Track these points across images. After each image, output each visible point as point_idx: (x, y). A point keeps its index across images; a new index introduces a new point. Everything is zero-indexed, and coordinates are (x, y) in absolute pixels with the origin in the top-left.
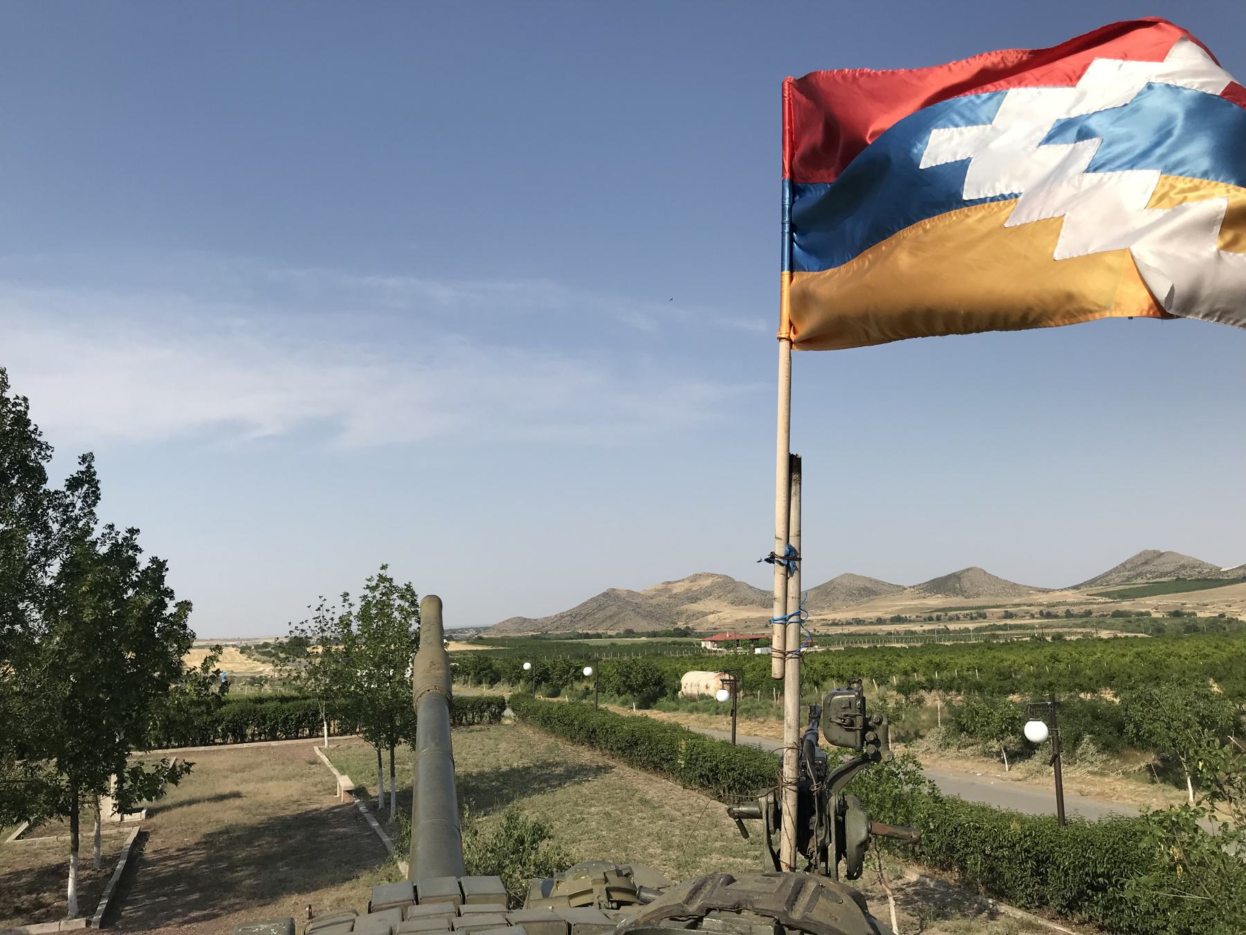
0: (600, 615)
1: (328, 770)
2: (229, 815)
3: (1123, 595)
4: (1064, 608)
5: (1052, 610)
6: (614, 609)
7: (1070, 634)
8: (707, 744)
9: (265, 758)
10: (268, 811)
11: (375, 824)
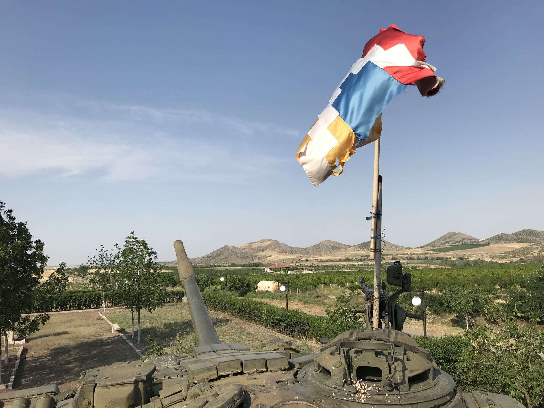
0: (221, 257)
1: (108, 322)
2: (63, 341)
3: (440, 251)
4: (416, 256)
5: (412, 257)
6: (227, 254)
7: (419, 266)
8: (275, 309)
9: (76, 317)
10: (82, 339)
11: (131, 344)
